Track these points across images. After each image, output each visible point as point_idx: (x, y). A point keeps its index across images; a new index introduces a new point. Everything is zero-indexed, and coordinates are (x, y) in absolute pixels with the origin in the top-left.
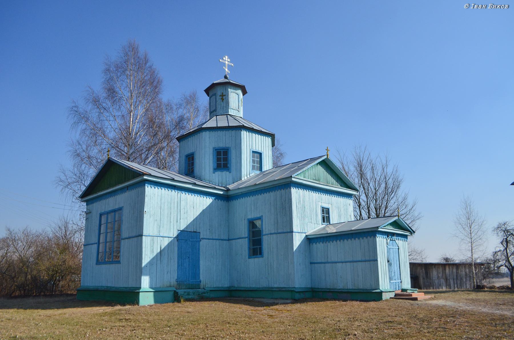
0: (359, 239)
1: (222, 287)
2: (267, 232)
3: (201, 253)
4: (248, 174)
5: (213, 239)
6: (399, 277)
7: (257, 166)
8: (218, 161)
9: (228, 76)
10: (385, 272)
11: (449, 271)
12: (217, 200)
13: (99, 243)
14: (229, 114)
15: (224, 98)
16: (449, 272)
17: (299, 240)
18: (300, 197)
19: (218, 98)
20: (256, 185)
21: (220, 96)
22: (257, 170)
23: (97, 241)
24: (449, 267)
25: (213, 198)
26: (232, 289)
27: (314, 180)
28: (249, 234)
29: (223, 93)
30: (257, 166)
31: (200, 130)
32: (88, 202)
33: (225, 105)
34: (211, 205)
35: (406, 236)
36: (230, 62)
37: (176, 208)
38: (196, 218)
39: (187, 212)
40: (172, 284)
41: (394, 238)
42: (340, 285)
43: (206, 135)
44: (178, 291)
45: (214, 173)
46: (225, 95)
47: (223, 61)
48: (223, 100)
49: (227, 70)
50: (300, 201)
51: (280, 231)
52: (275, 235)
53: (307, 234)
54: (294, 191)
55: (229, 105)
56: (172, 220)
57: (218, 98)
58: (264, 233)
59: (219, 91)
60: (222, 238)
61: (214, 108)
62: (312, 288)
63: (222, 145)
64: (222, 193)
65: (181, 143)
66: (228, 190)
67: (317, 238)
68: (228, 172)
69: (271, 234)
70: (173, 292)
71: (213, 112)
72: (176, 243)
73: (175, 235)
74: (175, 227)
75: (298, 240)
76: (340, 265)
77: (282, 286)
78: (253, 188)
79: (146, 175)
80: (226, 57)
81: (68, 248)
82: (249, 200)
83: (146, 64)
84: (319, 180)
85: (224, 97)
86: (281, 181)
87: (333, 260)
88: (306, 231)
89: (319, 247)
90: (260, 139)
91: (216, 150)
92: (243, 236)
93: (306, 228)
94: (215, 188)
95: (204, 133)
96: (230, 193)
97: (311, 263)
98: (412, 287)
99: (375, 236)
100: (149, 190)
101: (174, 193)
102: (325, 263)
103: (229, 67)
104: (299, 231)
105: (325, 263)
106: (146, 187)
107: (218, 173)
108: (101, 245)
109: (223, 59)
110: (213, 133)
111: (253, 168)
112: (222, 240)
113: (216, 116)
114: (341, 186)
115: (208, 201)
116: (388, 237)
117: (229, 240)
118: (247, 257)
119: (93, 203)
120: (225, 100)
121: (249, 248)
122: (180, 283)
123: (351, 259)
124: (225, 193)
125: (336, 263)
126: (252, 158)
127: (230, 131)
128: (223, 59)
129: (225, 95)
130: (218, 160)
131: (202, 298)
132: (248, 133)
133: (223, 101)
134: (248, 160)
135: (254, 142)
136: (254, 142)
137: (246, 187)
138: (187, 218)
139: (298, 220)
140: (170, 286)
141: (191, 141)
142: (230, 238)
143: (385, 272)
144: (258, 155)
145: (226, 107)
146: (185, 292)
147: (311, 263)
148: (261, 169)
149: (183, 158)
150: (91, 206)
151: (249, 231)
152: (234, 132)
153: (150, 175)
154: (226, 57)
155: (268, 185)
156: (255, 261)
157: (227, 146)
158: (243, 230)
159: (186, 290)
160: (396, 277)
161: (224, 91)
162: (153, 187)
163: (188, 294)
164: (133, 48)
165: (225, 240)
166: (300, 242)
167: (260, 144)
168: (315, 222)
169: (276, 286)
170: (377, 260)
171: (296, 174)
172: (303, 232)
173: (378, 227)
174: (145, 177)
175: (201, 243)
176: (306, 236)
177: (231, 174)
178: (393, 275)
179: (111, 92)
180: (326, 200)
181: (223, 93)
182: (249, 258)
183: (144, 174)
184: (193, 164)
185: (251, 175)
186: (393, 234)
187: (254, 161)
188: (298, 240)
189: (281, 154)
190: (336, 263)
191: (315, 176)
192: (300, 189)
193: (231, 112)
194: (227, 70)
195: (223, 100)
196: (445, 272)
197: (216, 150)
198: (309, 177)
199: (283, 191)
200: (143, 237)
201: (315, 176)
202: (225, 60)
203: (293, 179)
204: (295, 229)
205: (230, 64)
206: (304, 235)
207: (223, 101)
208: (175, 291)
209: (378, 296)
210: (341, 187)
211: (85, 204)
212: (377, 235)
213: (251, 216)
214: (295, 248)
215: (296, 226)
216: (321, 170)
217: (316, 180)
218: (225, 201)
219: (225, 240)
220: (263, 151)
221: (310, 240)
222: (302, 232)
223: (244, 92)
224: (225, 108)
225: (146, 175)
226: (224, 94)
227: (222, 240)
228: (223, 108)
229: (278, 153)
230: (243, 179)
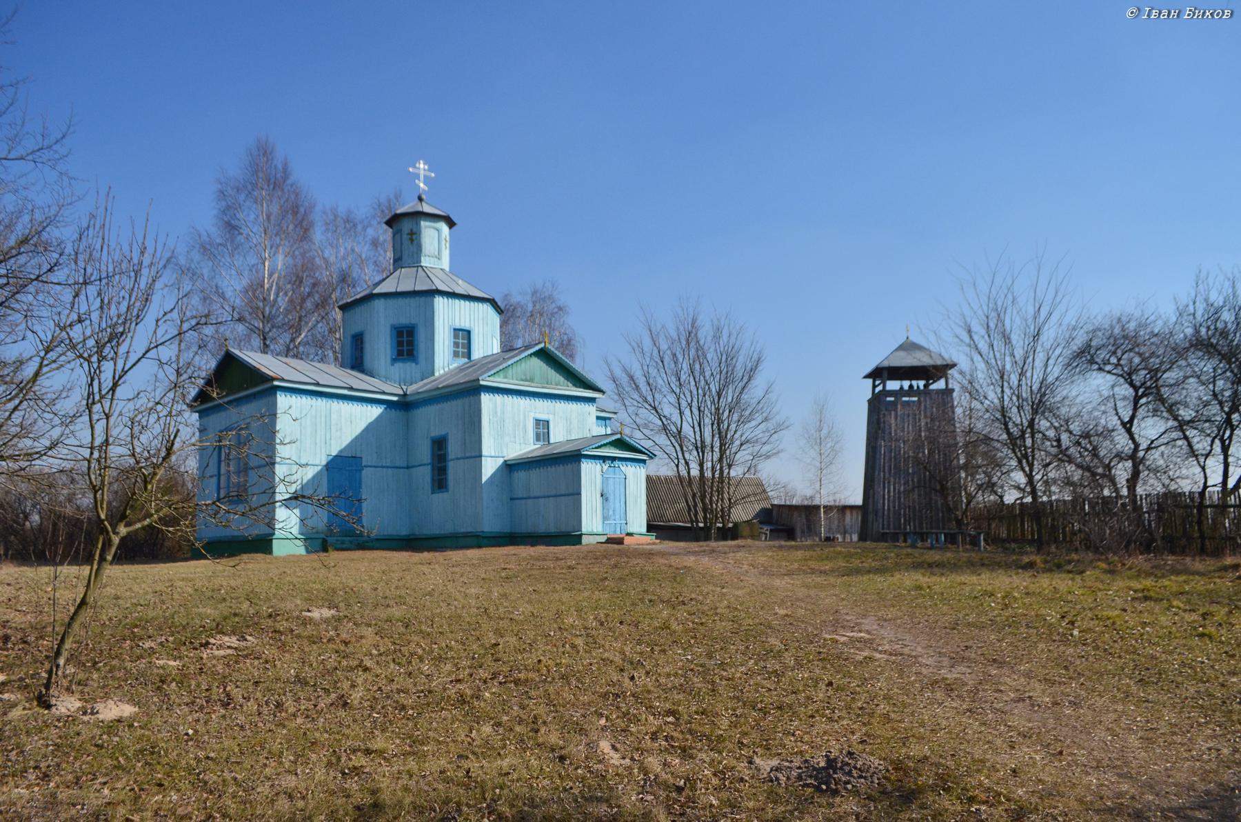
0: (563, 465)
1: (398, 535)
2: (453, 457)
3: (363, 486)
4: (446, 364)
5: (383, 467)
6: (623, 515)
7: (463, 352)
8: (398, 346)
9: (424, 197)
10: (594, 509)
11: (851, 519)
12: (388, 410)
13: (219, 475)
14: (422, 264)
15: (414, 237)
16: (851, 522)
17: (492, 467)
18: (496, 407)
19: (405, 237)
20: (438, 389)
21: (408, 234)
22: (463, 357)
23: (216, 473)
24: (852, 514)
25: (383, 407)
26: (411, 537)
27: (522, 380)
28: (433, 459)
29: (412, 230)
30: (463, 352)
31: (370, 297)
32: (202, 413)
33: (415, 250)
34: (380, 416)
35: (644, 461)
36: (429, 170)
37: (323, 424)
38: (356, 438)
39: (341, 429)
40: (320, 528)
41: (617, 463)
42: (542, 528)
43: (379, 304)
44: (328, 539)
45: (392, 365)
46: (415, 234)
47: (417, 171)
48: (412, 240)
49: (422, 185)
50: (496, 413)
51: (467, 455)
52: (462, 461)
53: (506, 459)
54: (485, 398)
55: (421, 251)
56: (318, 441)
57: (405, 237)
58: (450, 457)
59: (406, 226)
60: (397, 465)
61: (399, 255)
62: (511, 533)
63: (404, 321)
64: (395, 399)
65: (346, 314)
66: (405, 395)
67: (519, 464)
68: (414, 365)
69: (458, 459)
70: (320, 541)
71: (398, 262)
72: (326, 472)
73: (324, 463)
74: (323, 450)
75: (489, 468)
76: (542, 500)
77: (470, 530)
78: (435, 393)
79: (277, 379)
80: (421, 162)
81: (175, 485)
82: (433, 409)
83: (284, 182)
84: (531, 380)
85: (414, 237)
86: (469, 385)
87: (536, 494)
88: (505, 454)
89: (520, 475)
90: (467, 308)
91: (395, 328)
92: (425, 462)
93: (505, 450)
94: (384, 393)
95: (377, 301)
96: (409, 399)
97: (511, 499)
98: (648, 532)
99: (579, 462)
100: (283, 400)
101: (320, 403)
102: (526, 498)
103: (427, 180)
104: (493, 454)
105: (526, 498)
106: (278, 396)
107: (399, 365)
108: (223, 478)
109: (414, 167)
110: (392, 302)
111: (456, 354)
112: (397, 467)
113: (402, 268)
114: (575, 385)
115: (375, 411)
116: (604, 462)
117: (408, 468)
118: (430, 492)
119: (207, 415)
120: (415, 242)
121: (433, 480)
122: (330, 531)
123: (553, 493)
124: (402, 400)
125: (538, 498)
126: (452, 340)
127: (417, 299)
128: (414, 167)
129: (415, 234)
130: (400, 344)
131: (363, 546)
132: (446, 299)
133: (412, 243)
134: (446, 343)
135: (457, 314)
136: (457, 314)
137: (443, 387)
138: (340, 438)
139: (492, 441)
140: (317, 533)
141: (359, 311)
142: (410, 465)
143: (594, 509)
144: (463, 337)
145: (417, 253)
146: (337, 540)
147: (511, 499)
148: (469, 357)
149: (349, 338)
150: (206, 419)
151: (433, 455)
152: (422, 300)
153: (283, 380)
154: (421, 162)
155: (456, 388)
156: (439, 497)
157: (413, 322)
158: (424, 453)
159: (339, 538)
160: (617, 517)
161: (415, 226)
162: (289, 396)
163: (343, 542)
164: (265, 151)
165: (403, 468)
166: (494, 470)
167: (468, 316)
168: (522, 441)
169: (462, 530)
170: (579, 494)
171: (486, 375)
172: (500, 455)
173: (579, 450)
174: (276, 383)
175: (364, 472)
176: (505, 461)
177: (418, 366)
178: (611, 513)
179: (231, 228)
180: (542, 409)
181: (412, 230)
182: (432, 493)
183: (273, 379)
184: (362, 349)
185: (451, 367)
186: (613, 459)
187: (456, 345)
188: (489, 468)
189: (560, 309)
190: (538, 498)
191: (525, 375)
192: (496, 395)
193: (425, 262)
194: (422, 185)
195: (412, 240)
196: (844, 520)
197: (395, 328)
198: (514, 376)
199: (466, 400)
200: (483, 458)
201: (525, 375)
202: (419, 169)
203: (482, 383)
204: (485, 452)
205: (428, 173)
206: (501, 461)
207: (412, 243)
208: (324, 539)
209: (573, 538)
210: (575, 389)
211: (197, 415)
212: (583, 460)
213: (436, 432)
214: (484, 479)
215: (489, 446)
216: (537, 363)
217: (526, 380)
218: (403, 412)
219: (403, 468)
220: (472, 326)
221: (510, 467)
222: (497, 455)
223: (451, 224)
224: (415, 256)
225: (277, 379)
226: (414, 230)
227: (397, 467)
228: (413, 255)
229: (554, 305)
230: (437, 374)
